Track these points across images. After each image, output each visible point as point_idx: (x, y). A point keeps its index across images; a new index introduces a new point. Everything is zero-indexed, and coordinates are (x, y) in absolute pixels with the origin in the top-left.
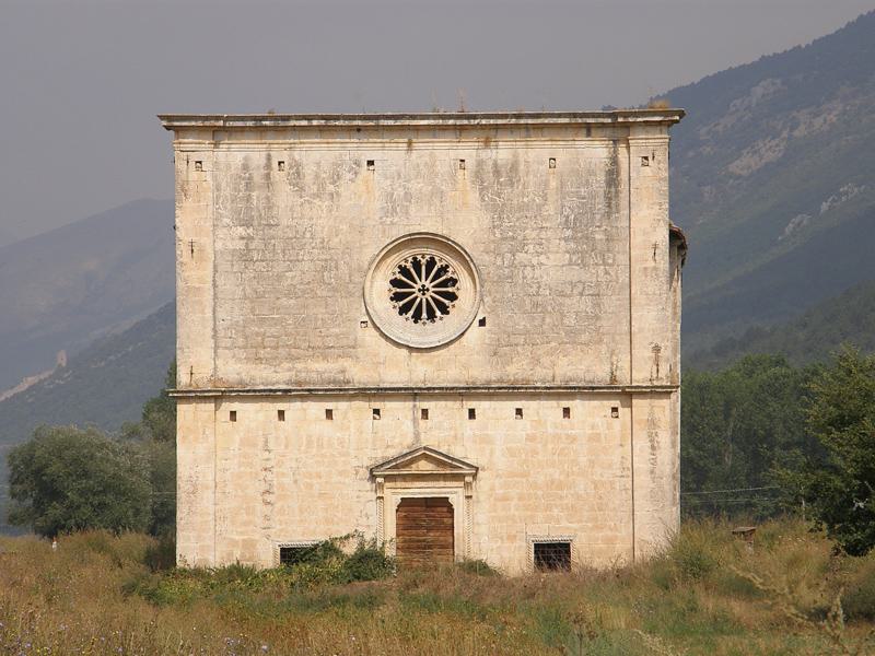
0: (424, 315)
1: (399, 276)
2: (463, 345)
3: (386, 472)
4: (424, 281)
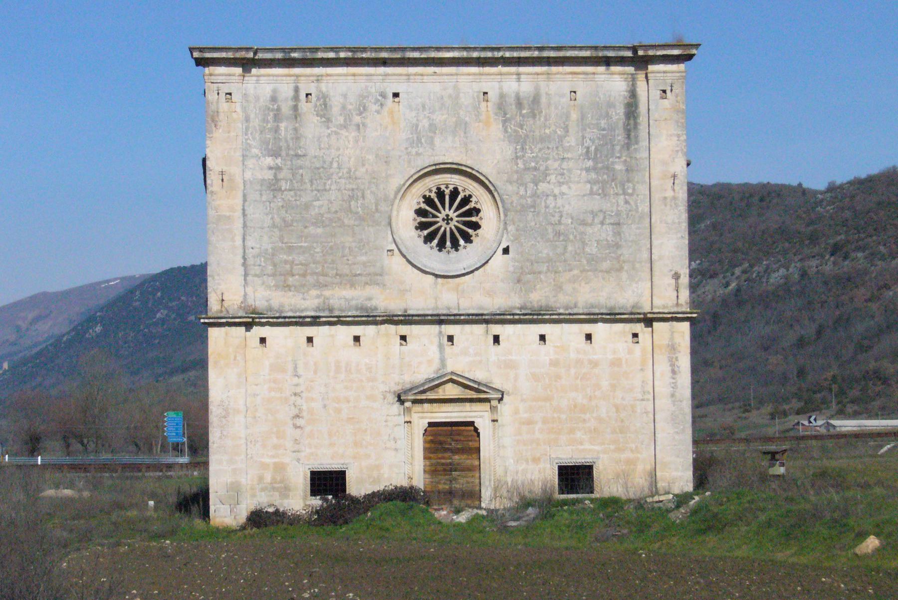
0: (448, 244)
1: (424, 206)
2: (485, 274)
3: (410, 397)
4: (448, 216)
